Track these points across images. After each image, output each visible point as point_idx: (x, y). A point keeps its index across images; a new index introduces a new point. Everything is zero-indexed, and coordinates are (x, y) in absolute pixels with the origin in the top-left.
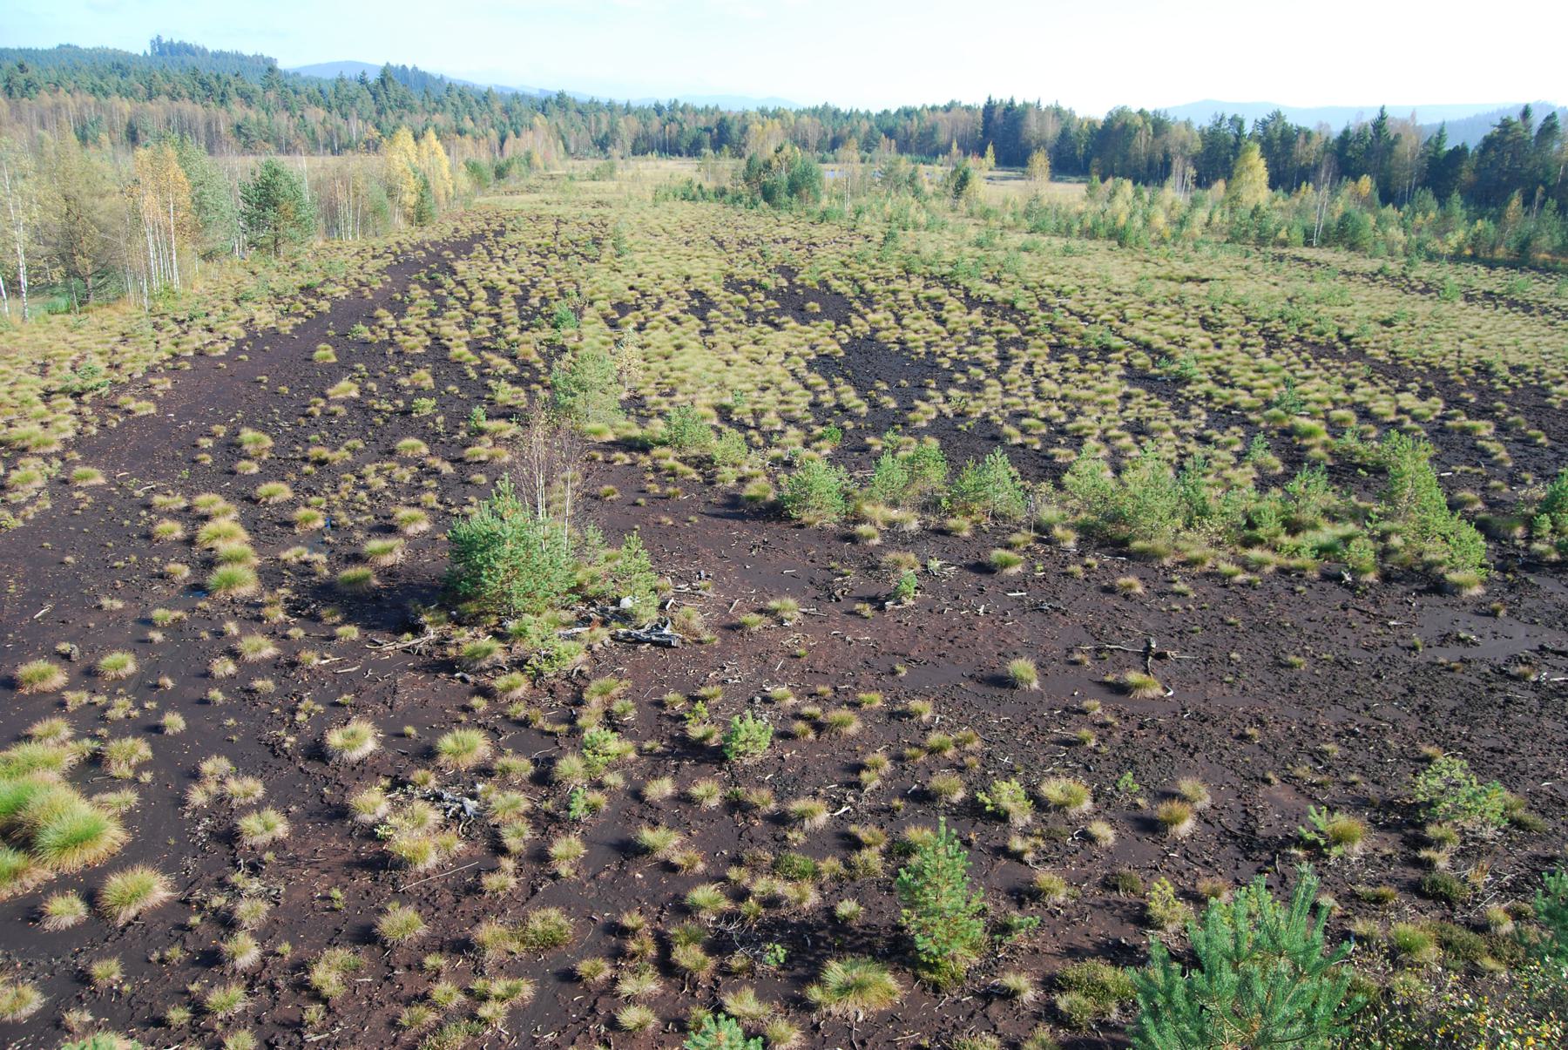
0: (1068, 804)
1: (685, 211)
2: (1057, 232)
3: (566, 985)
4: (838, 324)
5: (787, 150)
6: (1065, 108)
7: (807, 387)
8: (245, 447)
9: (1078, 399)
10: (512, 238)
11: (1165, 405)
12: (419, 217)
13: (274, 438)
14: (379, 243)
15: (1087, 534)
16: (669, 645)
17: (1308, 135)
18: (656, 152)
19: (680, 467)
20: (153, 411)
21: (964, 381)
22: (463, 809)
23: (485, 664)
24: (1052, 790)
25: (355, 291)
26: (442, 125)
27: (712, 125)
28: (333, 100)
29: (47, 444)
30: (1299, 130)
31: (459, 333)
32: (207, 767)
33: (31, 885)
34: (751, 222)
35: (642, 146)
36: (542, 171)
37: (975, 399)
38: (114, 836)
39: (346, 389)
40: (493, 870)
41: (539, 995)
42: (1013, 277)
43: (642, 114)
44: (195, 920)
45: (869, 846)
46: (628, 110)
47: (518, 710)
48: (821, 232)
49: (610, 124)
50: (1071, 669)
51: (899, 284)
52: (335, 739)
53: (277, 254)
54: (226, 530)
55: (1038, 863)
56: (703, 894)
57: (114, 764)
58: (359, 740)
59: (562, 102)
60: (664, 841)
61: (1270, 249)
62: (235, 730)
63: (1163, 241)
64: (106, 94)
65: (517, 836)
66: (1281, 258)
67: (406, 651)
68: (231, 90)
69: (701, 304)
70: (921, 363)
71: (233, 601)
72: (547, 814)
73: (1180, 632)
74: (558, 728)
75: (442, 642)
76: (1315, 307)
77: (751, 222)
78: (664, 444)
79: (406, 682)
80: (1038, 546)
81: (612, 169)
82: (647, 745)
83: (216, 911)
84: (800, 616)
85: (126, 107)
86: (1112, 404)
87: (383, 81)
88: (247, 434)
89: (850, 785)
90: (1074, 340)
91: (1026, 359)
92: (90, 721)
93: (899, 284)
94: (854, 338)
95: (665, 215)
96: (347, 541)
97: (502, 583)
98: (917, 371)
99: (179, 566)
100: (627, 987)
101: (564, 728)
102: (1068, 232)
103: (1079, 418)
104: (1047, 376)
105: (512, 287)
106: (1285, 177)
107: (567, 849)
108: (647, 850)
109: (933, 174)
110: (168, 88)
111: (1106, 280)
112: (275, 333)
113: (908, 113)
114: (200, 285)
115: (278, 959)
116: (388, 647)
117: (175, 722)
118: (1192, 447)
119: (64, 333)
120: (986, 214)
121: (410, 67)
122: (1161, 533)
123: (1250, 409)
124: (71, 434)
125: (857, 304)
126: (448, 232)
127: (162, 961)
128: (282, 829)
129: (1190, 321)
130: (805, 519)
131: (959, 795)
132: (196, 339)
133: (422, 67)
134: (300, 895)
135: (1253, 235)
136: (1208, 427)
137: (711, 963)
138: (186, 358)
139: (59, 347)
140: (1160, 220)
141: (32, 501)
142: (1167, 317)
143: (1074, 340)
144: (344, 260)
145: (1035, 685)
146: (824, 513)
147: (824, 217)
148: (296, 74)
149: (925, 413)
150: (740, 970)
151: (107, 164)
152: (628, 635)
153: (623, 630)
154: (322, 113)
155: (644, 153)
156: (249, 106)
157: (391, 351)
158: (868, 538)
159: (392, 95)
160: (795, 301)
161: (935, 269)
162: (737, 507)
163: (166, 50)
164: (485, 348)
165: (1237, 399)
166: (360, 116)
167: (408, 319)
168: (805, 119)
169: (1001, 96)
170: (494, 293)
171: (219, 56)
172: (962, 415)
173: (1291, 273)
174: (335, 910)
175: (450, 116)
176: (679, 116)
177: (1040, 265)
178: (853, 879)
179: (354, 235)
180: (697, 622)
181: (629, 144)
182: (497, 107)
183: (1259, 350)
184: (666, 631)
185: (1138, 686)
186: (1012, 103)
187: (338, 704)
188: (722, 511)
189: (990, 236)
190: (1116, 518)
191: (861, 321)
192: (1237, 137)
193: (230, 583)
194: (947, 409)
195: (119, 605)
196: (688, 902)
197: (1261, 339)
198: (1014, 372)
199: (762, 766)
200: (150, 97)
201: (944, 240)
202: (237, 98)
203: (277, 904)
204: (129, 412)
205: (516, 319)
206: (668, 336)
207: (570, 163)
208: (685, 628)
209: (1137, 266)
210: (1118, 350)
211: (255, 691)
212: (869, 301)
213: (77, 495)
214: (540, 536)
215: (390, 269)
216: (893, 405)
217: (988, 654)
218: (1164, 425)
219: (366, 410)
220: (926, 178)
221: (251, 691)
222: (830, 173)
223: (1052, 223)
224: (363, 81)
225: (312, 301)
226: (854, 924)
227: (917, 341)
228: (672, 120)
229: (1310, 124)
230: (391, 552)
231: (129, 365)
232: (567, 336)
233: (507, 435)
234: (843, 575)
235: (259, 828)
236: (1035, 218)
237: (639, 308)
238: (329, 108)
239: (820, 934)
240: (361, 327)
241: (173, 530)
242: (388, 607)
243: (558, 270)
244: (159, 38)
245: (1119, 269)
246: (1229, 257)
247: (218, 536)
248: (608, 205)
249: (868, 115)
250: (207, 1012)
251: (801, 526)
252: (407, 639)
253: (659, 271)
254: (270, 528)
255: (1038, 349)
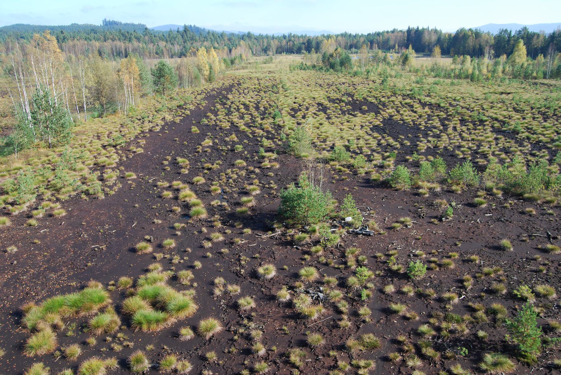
0: (548, 295)
1: (303, 74)
2: (445, 77)
3: (385, 363)
4: (376, 114)
5: (339, 49)
6: (438, 29)
7: (374, 138)
8: (180, 164)
9: (478, 140)
10: (245, 86)
11: (513, 142)
12: (210, 79)
13: (189, 160)
14: (199, 89)
15: (506, 192)
16: (370, 235)
17: (538, 35)
18: (285, 53)
19: (343, 169)
20: (142, 151)
21: (432, 134)
22: (318, 296)
23: (304, 242)
24: (540, 289)
25: (197, 107)
26: (207, 46)
27: (305, 41)
28: (168, 38)
29: (112, 164)
30: (534, 34)
31: (240, 121)
32: (217, 281)
33: (170, 324)
34: (328, 77)
35: (280, 50)
36: (246, 61)
37: (439, 141)
38: (193, 308)
39: (208, 142)
40: (341, 320)
41: (377, 366)
42: (435, 95)
43: (278, 38)
44: (236, 337)
45: (479, 310)
46: (273, 38)
47: (323, 260)
48: (356, 80)
49: (267, 43)
50: (523, 243)
51: (393, 98)
52: (261, 270)
53: (164, 94)
54: (187, 194)
55: (545, 317)
56: (424, 328)
57: (182, 280)
58: (269, 271)
59: (249, 36)
60: (401, 308)
61: (530, 80)
62: (220, 267)
63: (488, 79)
64: (90, 40)
65: (344, 306)
66: (536, 84)
67: (271, 238)
68: (133, 37)
69: (323, 108)
70: (412, 128)
71: (200, 220)
72: (350, 298)
73: (557, 229)
74: (340, 266)
75: (284, 234)
76: (557, 102)
77: (328, 77)
78: (333, 160)
79: (276, 249)
80: (488, 197)
81: (271, 59)
82: (377, 273)
83: (242, 334)
84: (412, 224)
85: (97, 44)
86: (492, 142)
87: (185, 31)
88: (180, 159)
89: (461, 288)
90: (468, 118)
91: (452, 126)
92: (167, 264)
93: (393, 98)
94: (384, 119)
95: (296, 75)
96: (232, 197)
97: (304, 212)
98: (412, 131)
99: (177, 207)
100: (410, 363)
101: (342, 266)
102: (449, 77)
103: (482, 147)
104: (463, 132)
105: (251, 104)
106: (532, 53)
107: (364, 311)
108: (396, 312)
109: (392, 56)
110: (111, 37)
111: (472, 94)
112: (174, 123)
113: (378, 34)
114: (141, 106)
115: (273, 352)
116: (264, 237)
117: (198, 264)
118: (530, 158)
119: (101, 125)
120: (416, 71)
121: (193, 25)
122: (537, 191)
123: (547, 143)
124: (117, 160)
125: (380, 106)
126: (221, 84)
127: (229, 352)
128: (253, 305)
129: (510, 109)
130: (398, 187)
131: (504, 292)
132: (147, 126)
133: (197, 25)
134: (270, 329)
135: (524, 75)
136: (532, 150)
137: (438, 354)
138: (147, 132)
139: (101, 130)
140: (485, 71)
141: (115, 184)
142: (500, 108)
143: (468, 118)
144: (190, 95)
145: (512, 249)
146: (404, 185)
147: (355, 74)
148: (153, 30)
149: (424, 146)
150: (451, 357)
151: (110, 66)
152: (353, 231)
153: (351, 230)
154: (164, 43)
155: (280, 53)
156: (139, 42)
157: (218, 128)
158: (424, 194)
159: (189, 36)
160: (357, 106)
161: (404, 92)
162: (368, 183)
163: (109, 24)
164: (252, 126)
165: (540, 139)
166: (178, 44)
167: (220, 116)
168: (340, 38)
169: (414, 26)
170: (247, 107)
171: (126, 25)
172: (436, 147)
173: (542, 89)
174: (286, 334)
175: (209, 42)
176: (293, 39)
177: (445, 90)
178: (478, 323)
179: (188, 87)
180: (376, 226)
181: (275, 50)
182: (226, 38)
183: (541, 119)
184: (367, 230)
185: (552, 250)
186: (418, 28)
187: (254, 258)
188: (364, 185)
189: (421, 79)
190: (516, 185)
191: (385, 113)
192: (509, 37)
193: (198, 213)
194: (430, 145)
195: (160, 222)
196: (419, 331)
197: (540, 116)
198: (450, 130)
199: (424, 280)
200: (105, 41)
201: (404, 82)
202: (135, 39)
203: (264, 332)
204: (135, 152)
205: (258, 115)
206: (316, 120)
207: (255, 58)
208: (373, 229)
209: (481, 89)
210: (486, 121)
211: (222, 253)
212: (384, 105)
213: (129, 182)
214: (313, 196)
215: (205, 99)
216: (409, 144)
217: (488, 237)
218: (516, 149)
219: (217, 150)
220: (390, 58)
221: (221, 253)
222: (354, 58)
223: (443, 74)
224: (178, 32)
225: (183, 111)
226: (486, 340)
227: (408, 119)
228: (290, 40)
229: (537, 31)
230: (250, 201)
231: (128, 135)
232: (278, 121)
233: (273, 158)
234: (421, 208)
235: (246, 304)
236: (435, 71)
237: (300, 110)
238: (167, 41)
239: (474, 343)
240: (205, 120)
241: (169, 194)
242: (260, 221)
243: (265, 97)
244: (105, 20)
245: (476, 90)
246: (515, 84)
247: (186, 196)
248: (274, 72)
249: (362, 35)
250: (256, 372)
251: (397, 190)
252: (270, 234)
253: (303, 96)
254: (204, 193)
255: (456, 121)
